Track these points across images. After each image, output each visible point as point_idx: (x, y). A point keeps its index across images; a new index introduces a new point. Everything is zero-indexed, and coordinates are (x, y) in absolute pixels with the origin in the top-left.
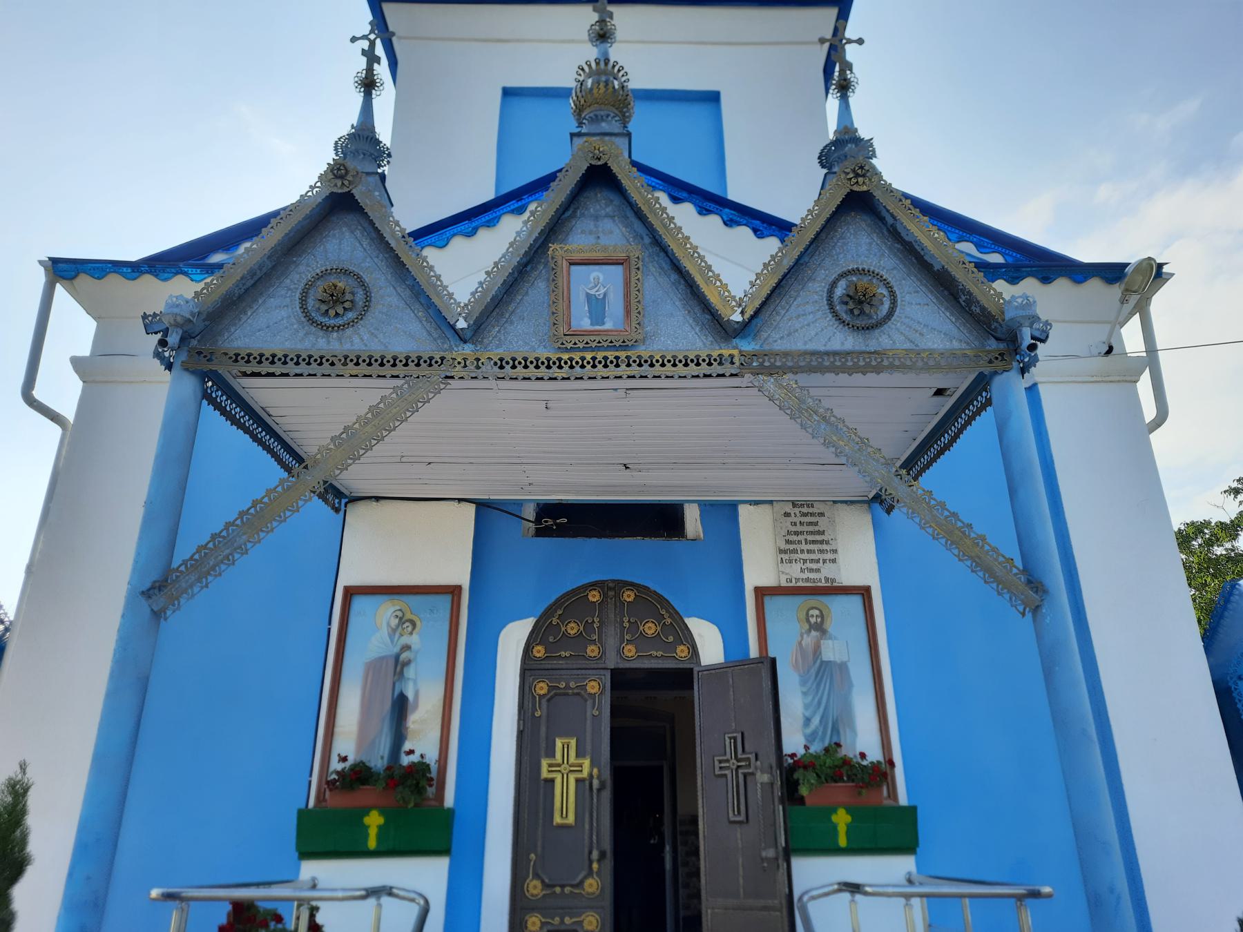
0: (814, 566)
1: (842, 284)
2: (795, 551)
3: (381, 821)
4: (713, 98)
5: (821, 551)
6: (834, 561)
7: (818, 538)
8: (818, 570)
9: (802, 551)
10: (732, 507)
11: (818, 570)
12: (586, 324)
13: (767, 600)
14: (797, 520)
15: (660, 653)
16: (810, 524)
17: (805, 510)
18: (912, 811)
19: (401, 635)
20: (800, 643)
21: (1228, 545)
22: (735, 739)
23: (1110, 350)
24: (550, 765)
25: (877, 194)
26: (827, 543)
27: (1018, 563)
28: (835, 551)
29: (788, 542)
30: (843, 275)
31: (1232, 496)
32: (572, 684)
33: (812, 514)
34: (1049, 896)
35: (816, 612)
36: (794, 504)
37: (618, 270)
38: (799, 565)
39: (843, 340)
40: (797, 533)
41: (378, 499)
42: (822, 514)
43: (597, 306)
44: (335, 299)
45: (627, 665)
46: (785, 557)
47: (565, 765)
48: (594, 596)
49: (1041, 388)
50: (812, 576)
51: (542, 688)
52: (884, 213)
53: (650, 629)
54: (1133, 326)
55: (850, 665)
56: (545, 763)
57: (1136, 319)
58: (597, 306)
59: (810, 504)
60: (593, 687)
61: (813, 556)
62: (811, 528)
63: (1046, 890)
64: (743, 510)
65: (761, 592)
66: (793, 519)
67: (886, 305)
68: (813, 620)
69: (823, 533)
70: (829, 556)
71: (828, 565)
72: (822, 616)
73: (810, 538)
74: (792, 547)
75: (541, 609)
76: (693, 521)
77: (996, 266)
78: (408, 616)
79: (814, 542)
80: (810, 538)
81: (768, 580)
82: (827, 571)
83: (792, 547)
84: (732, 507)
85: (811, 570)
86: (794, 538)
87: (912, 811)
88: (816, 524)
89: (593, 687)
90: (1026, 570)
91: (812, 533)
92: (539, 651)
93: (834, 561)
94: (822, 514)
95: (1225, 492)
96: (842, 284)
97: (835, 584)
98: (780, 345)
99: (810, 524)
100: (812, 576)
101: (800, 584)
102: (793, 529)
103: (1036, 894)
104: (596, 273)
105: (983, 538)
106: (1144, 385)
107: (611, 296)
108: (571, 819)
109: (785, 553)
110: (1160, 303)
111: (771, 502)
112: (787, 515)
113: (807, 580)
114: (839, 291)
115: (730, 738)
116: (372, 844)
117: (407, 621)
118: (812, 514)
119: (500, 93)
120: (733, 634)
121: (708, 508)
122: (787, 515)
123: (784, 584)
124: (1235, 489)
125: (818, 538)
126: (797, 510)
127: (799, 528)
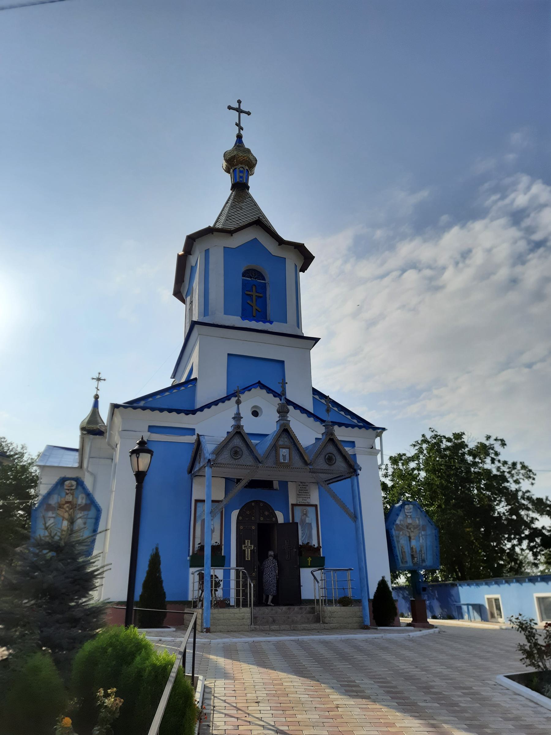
0: (305, 499)
1: (327, 456)
2: (301, 495)
4: (282, 362)
5: (307, 495)
6: (309, 498)
7: (306, 492)
8: (306, 500)
9: (303, 495)
10: (287, 482)
11: (306, 500)
12: (282, 461)
13: (294, 507)
14: (302, 487)
15: (269, 520)
16: (305, 488)
17: (303, 484)
18: (324, 558)
20: (301, 518)
22: (288, 541)
23: (372, 448)
24: (244, 546)
25: (334, 439)
26: (308, 493)
27: (353, 513)
28: (310, 495)
29: (299, 492)
30: (327, 454)
31: (413, 447)
32: (249, 527)
33: (305, 485)
34: (353, 570)
36: (301, 482)
37: (288, 449)
38: (301, 499)
39: (326, 467)
40: (301, 490)
41: (201, 476)
42: (307, 486)
43: (284, 456)
44: (236, 453)
45: (261, 522)
46: (299, 496)
48: (253, 504)
49: (357, 455)
50: (305, 501)
51: (241, 528)
53: (266, 513)
54: (378, 440)
56: (243, 546)
57: (379, 438)
58: (284, 456)
59: (305, 483)
60: (253, 528)
61: (305, 496)
62: (305, 489)
63: (353, 569)
64: (289, 483)
65: (293, 505)
66: (301, 486)
67: (334, 462)
68: (304, 513)
69: (307, 490)
71: (308, 499)
72: (306, 512)
73: (304, 492)
74: (300, 494)
75: (241, 507)
76: (276, 485)
79: (306, 493)
80: (304, 492)
81: (294, 502)
82: (308, 500)
83: (300, 494)
84: (287, 482)
86: (301, 491)
87: (324, 558)
88: (306, 488)
89: (253, 528)
90: (355, 514)
91: (305, 490)
92: (241, 518)
93: (309, 498)
94: (307, 486)
95: (411, 445)
96: (327, 456)
99: (305, 488)
100: (305, 501)
101: (302, 503)
102: (301, 489)
103: (351, 569)
104: (284, 450)
105: (348, 508)
106: (379, 456)
107: (287, 455)
108: (249, 559)
109: (298, 495)
110: (384, 434)
111: (296, 482)
112: (299, 485)
113: (304, 502)
114: (327, 457)
118: (305, 485)
119: (227, 355)
120: (286, 516)
121: (280, 482)
122: (299, 485)
123: (298, 503)
124: (414, 445)
125: (306, 492)
127: (302, 489)
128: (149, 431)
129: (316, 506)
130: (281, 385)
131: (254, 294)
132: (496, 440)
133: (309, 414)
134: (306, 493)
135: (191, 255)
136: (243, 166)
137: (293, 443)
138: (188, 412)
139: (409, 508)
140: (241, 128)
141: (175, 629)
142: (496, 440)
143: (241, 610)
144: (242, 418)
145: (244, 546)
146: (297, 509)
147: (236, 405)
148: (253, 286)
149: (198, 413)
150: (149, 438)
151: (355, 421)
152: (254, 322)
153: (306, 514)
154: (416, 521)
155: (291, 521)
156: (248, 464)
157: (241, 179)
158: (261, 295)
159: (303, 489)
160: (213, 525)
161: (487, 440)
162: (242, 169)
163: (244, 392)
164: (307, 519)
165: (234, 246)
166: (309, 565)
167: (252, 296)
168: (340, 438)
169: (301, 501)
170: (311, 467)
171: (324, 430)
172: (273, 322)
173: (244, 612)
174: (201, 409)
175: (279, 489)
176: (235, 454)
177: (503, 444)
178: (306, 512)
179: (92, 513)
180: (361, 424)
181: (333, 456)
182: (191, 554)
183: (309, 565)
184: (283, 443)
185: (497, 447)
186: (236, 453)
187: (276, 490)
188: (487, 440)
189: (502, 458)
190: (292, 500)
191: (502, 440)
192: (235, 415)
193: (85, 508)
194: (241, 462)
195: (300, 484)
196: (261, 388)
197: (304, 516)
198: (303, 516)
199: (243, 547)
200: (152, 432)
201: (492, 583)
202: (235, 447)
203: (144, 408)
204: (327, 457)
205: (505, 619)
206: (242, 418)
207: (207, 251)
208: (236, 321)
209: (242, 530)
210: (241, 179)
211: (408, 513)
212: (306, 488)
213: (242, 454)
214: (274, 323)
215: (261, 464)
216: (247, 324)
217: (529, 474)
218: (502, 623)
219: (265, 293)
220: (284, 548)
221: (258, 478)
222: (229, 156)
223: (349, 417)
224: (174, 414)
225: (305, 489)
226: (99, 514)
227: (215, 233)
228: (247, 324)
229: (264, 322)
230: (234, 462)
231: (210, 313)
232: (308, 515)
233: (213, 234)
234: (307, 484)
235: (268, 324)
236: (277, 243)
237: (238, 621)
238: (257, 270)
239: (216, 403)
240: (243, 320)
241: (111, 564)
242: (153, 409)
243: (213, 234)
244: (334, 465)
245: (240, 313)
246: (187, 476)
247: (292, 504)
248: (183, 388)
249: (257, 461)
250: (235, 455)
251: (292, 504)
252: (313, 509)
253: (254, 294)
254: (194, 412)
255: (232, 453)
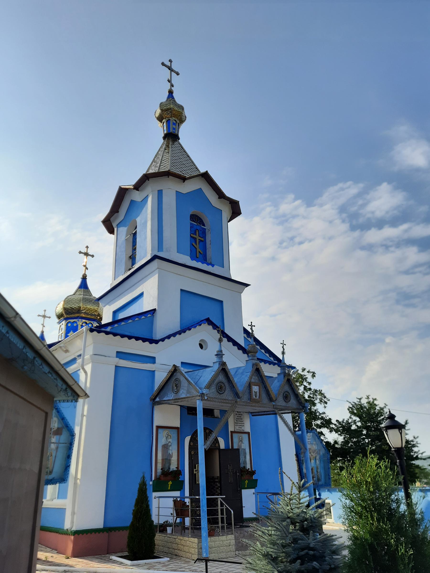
0: (241, 427)
2: (238, 423)
3: (171, 483)
4: (221, 302)
5: (242, 423)
7: (241, 420)
11: (241, 428)
17: (239, 413)
19: (168, 439)
21: (84, 297)
24: (195, 471)
28: (244, 424)
35: (241, 437)
38: (238, 427)
40: (238, 419)
42: (242, 415)
44: (221, 388)
46: (236, 424)
47: (230, 470)
52: (290, 382)
55: (246, 449)
56: (195, 470)
58: (256, 393)
59: (240, 412)
68: (240, 439)
70: (243, 425)
72: (242, 438)
73: (240, 420)
74: (237, 422)
77: (275, 363)
78: (169, 434)
79: (241, 421)
81: (233, 430)
83: (237, 422)
85: (240, 428)
86: (237, 420)
88: (241, 417)
93: (244, 426)
96: (285, 394)
97: (244, 431)
98: (278, 404)
101: (239, 431)
102: (237, 418)
109: (236, 424)
113: (239, 430)
114: (284, 395)
115: (230, 465)
116: (169, 488)
117: (169, 435)
122: (236, 414)
123: (236, 431)
125: (241, 420)
126: (238, 413)
128: (117, 357)
129: (248, 433)
130: (251, 327)
131: (198, 238)
132: (308, 372)
133: (240, 347)
134: (241, 421)
135: (138, 191)
136: (176, 120)
137: (261, 381)
138: (271, 363)
139: (310, 436)
140: (172, 86)
141: (168, 559)
142: (308, 372)
143: (227, 537)
144: (224, 355)
145: (195, 471)
146: (235, 435)
147: (219, 343)
148: (197, 230)
149: (161, 343)
150: (117, 364)
151: (272, 359)
152: (200, 263)
153: (241, 441)
154: (313, 446)
155: (230, 448)
156: (230, 399)
157: (174, 131)
158: (202, 239)
159: (239, 419)
160: (172, 451)
161: (303, 371)
162: (175, 122)
163: (196, 326)
164: (242, 444)
165: (184, 192)
166: (246, 487)
167: (195, 239)
168: (266, 374)
169: (237, 429)
170: (274, 404)
171: (280, 370)
172: (214, 265)
173: (230, 539)
174: (163, 340)
175: (220, 417)
176: (220, 388)
177: (314, 375)
178: (242, 438)
179: (64, 437)
180: (276, 362)
181: (289, 395)
182: (153, 479)
183: (246, 487)
184: (254, 380)
185: (309, 377)
186: (220, 389)
187: (216, 418)
188: (303, 371)
189: (313, 387)
190: (231, 428)
191: (314, 373)
192: (217, 352)
193: (58, 432)
194: (224, 396)
195: (237, 413)
196: (209, 324)
197: (240, 442)
198: (240, 442)
199: (194, 471)
200: (120, 358)
201: (326, 490)
202: (220, 382)
203: (107, 333)
204: (284, 395)
205: (334, 519)
206: (224, 355)
207: (160, 192)
208: (186, 260)
209: (193, 454)
210: (174, 131)
211: (308, 439)
212: (241, 417)
213: (225, 389)
214: (215, 266)
215: (239, 400)
216: (194, 264)
217: (324, 401)
218: (331, 523)
219: (205, 237)
220: (227, 472)
221: (206, 407)
222: (165, 108)
223: (267, 355)
224: (126, 339)
225: (239, 418)
226: (73, 439)
227: (170, 177)
228: (194, 264)
229: (203, 263)
230: (219, 396)
231: (164, 250)
232: (244, 442)
233: (168, 177)
234: (241, 413)
235: (210, 266)
236: (217, 196)
237: (225, 548)
238: (199, 217)
239: (174, 335)
240: (192, 260)
241: (342, 537)
242: (115, 335)
243: (168, 177)
244: (289, 402)
245: (189, 253)
246: (148, 402)
247: (231, 432)
248: (143, 317)
249: (236, 396)
250: (220, 390)
251: (231, 432)
252: (246, 435)
253: (198, 238)
254: (157, 342)
255: (218, 388)
